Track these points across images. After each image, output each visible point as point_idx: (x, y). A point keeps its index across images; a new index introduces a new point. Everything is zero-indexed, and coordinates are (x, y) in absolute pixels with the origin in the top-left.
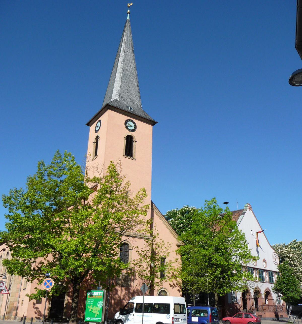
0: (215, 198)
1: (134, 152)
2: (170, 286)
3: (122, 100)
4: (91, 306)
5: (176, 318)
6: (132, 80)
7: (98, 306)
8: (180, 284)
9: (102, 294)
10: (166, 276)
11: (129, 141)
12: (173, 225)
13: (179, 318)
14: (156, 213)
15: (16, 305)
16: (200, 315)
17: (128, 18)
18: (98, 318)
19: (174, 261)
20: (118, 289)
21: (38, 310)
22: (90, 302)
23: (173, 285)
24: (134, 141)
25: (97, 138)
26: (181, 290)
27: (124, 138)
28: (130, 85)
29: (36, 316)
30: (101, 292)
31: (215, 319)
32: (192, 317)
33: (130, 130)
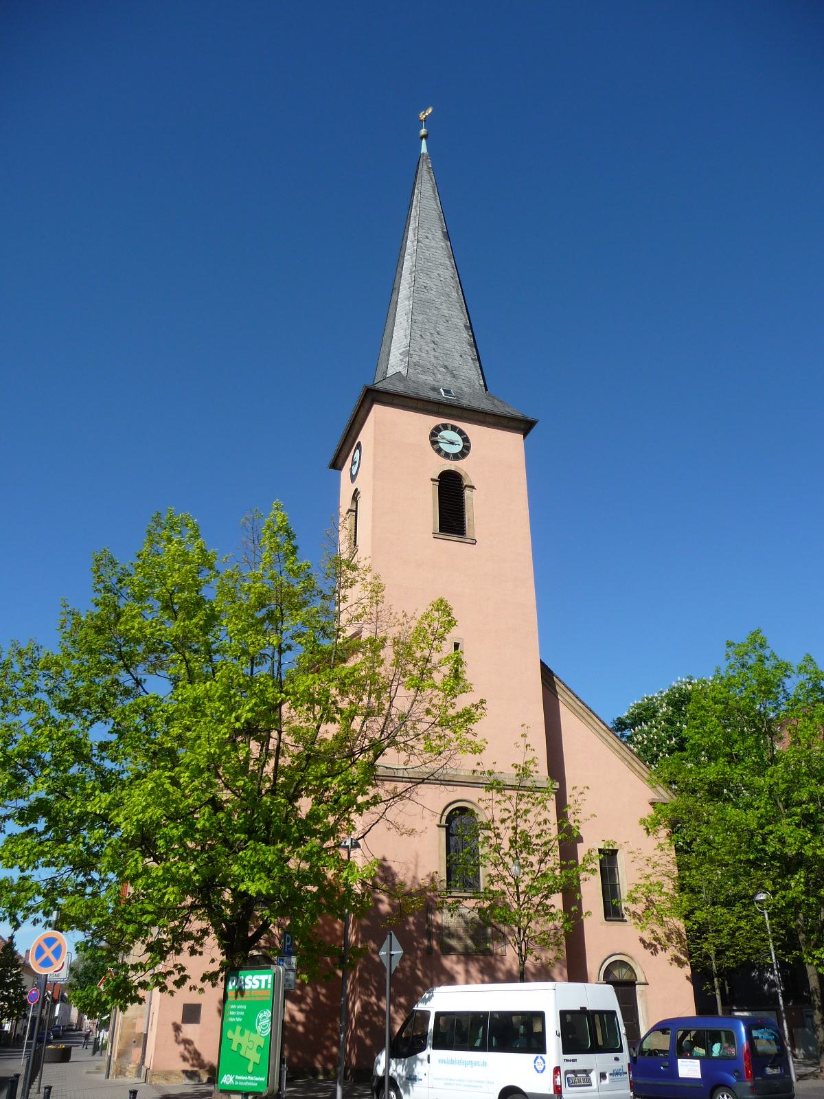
0: (759, 632)
1: (469, 520)
2: (645, 947)
3: (418, 373)
4: (239, 1028)
5: (574, 1072)
6: (446, 312)
7: (259, 1029)
8: (680, 935)
9: (270, 981)
10: (624, 912)
11: (451, 492)
12: (645, 743)
13: (586, 1072)
14: (568, 705)
15: (140, 1029)
16: (709, 1051)
17: (424, 149)
18: (257, 1079)
19: (647, 861)
20: (452, 968)
21: (191, 1048)
22: (235, 1016)
23: (654, 942)
24: (466, 486)
25: (356, 493)
26: (684, 958)
27: (433, 480)
28: (441, 328)
29: (187, 1066)
30: (265, 974)
31: (772, 1067)
32: (680, 1061)
33: (442, 453)
